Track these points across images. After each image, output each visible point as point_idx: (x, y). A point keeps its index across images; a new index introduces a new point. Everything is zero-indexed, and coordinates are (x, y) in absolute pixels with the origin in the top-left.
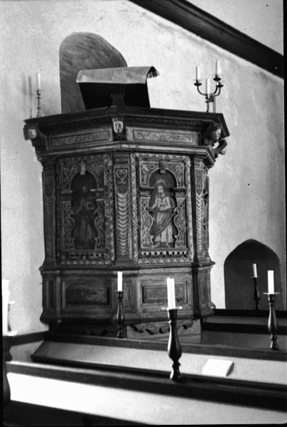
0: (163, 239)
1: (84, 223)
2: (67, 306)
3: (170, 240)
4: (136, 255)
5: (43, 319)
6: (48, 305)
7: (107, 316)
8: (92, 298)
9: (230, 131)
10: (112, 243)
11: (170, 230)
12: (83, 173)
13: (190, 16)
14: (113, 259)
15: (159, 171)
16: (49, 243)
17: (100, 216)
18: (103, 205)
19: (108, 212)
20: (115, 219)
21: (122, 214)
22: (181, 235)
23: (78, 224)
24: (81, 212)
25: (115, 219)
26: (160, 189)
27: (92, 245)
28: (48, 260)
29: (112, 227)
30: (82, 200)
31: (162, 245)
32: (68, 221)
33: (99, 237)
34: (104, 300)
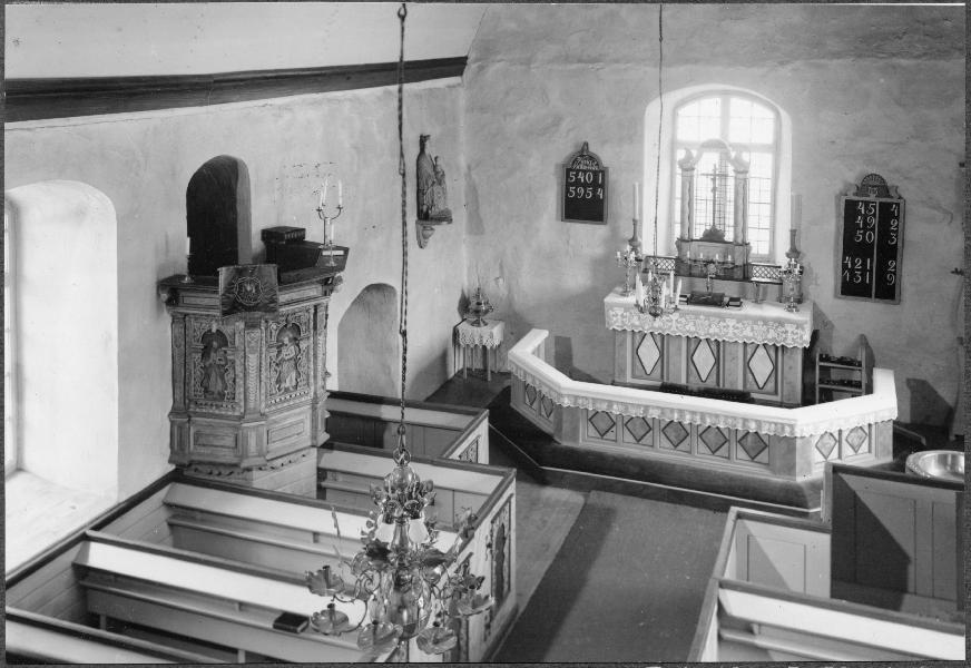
0: (287, 384)
1: (213, 374)
2: (195, 448)
3: (294, 383)
4: (263, 405)
5: (170, 461)
6: (176, 447)
7: (235, 461)
8: (222, 443)
9: (300, 226)
10: (242, 396)
11: (294, 375)
12: (214, 330)
13: (193, 299)
14: (242, 410)
15: (286, 326)
16: (177, 391)
17: (231, 371)
18: (233, 362)
19: (239, 369)
20: (245, 376)
21: (253, 373)
22: (303, 377)
23: (208, 376)
24: (211, 365)
25: (245, 376)
26: (286, 340)
27: (222, 396)
28: (176, 406)
29: (242, 382)
30: (213, 354)
31: (287, 390)
32: (196, 373)
33: (229, 390)
34: (233, 445)
